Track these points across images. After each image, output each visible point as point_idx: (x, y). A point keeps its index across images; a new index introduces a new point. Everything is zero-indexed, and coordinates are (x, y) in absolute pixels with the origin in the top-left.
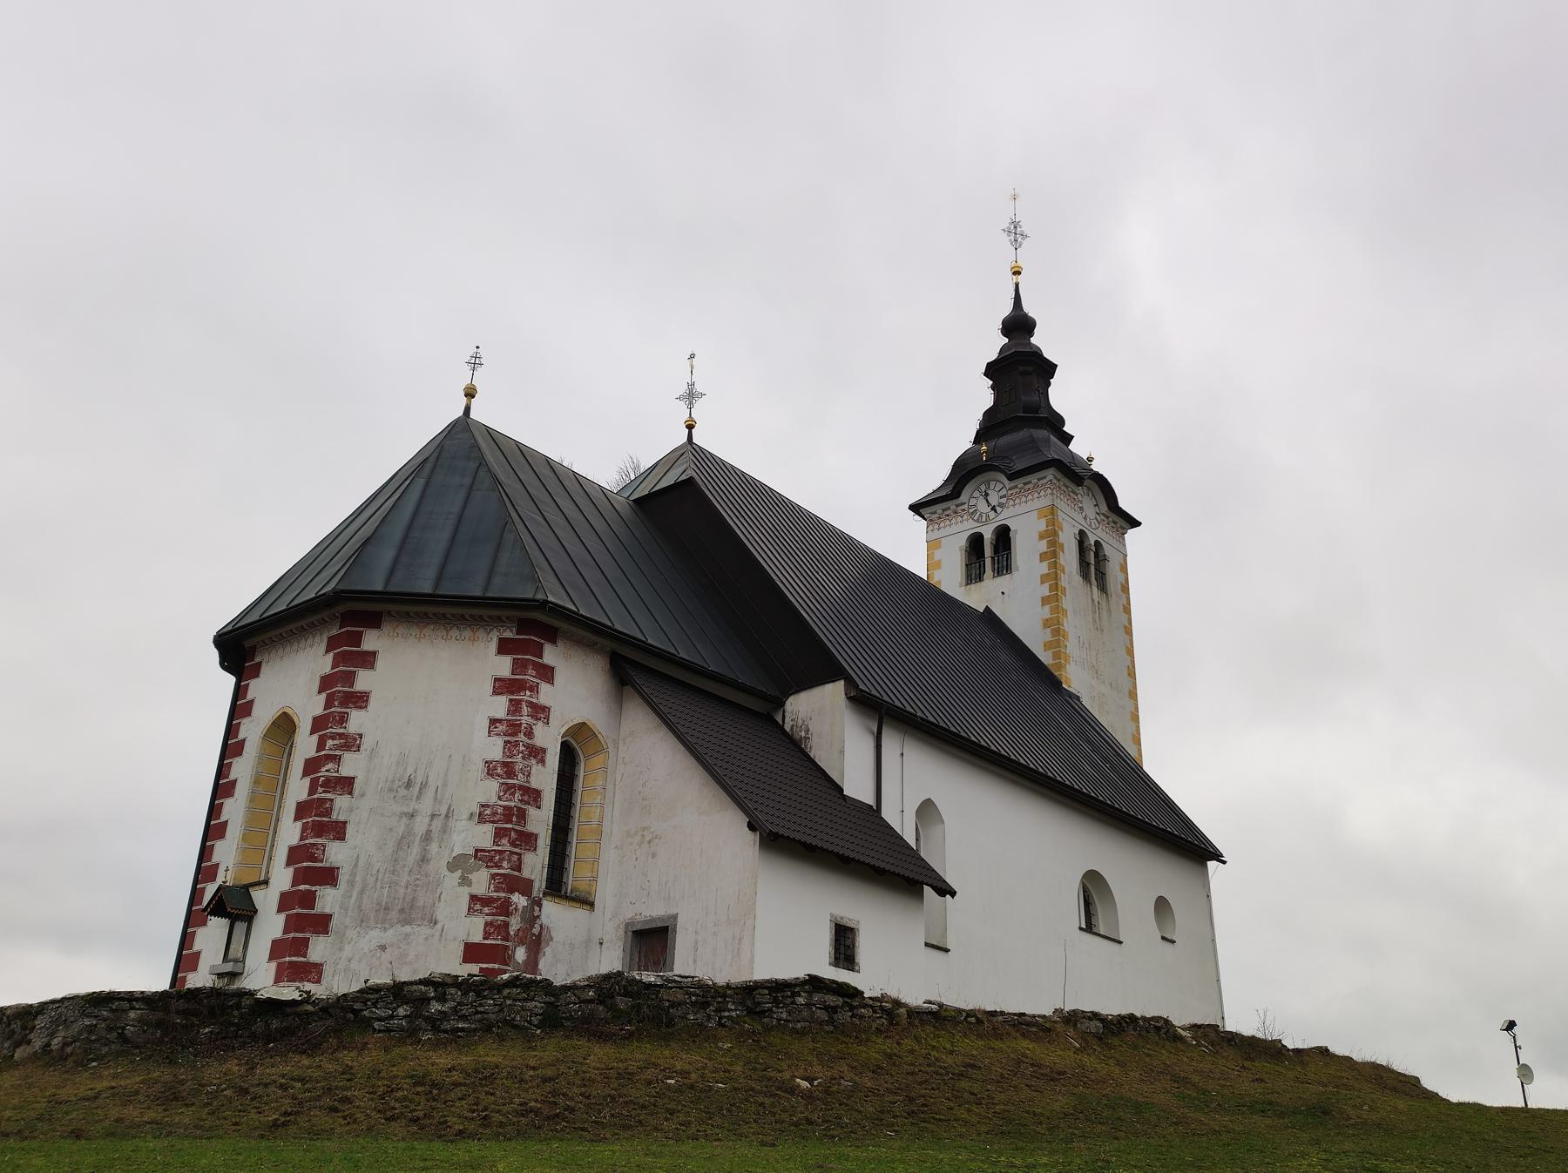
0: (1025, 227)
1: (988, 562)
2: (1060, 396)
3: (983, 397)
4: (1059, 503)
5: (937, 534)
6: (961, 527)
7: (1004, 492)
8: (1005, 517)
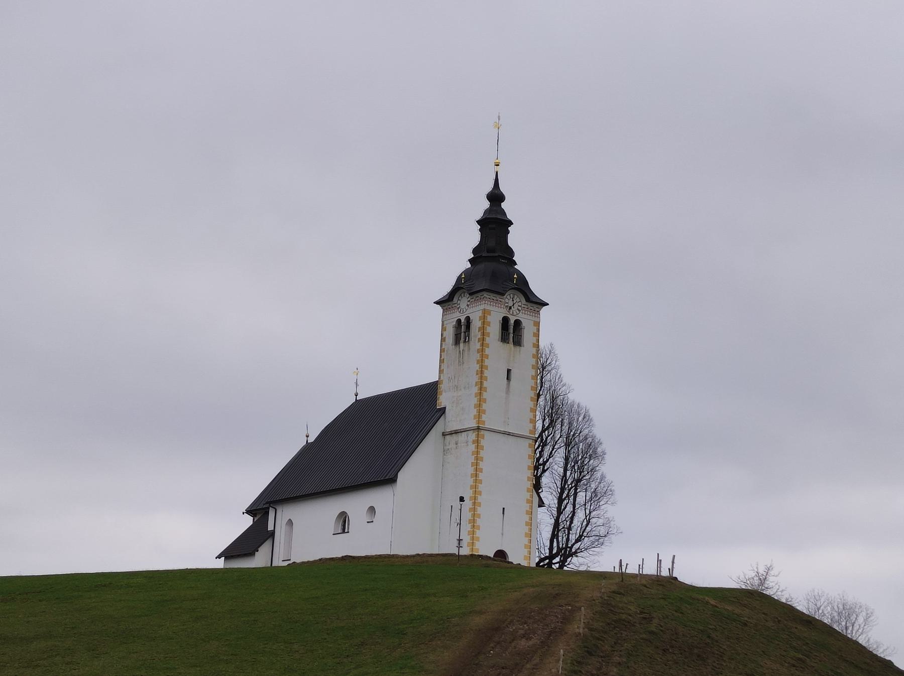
2: (513, 240)
3: (474, 237)
8: (522, 317)
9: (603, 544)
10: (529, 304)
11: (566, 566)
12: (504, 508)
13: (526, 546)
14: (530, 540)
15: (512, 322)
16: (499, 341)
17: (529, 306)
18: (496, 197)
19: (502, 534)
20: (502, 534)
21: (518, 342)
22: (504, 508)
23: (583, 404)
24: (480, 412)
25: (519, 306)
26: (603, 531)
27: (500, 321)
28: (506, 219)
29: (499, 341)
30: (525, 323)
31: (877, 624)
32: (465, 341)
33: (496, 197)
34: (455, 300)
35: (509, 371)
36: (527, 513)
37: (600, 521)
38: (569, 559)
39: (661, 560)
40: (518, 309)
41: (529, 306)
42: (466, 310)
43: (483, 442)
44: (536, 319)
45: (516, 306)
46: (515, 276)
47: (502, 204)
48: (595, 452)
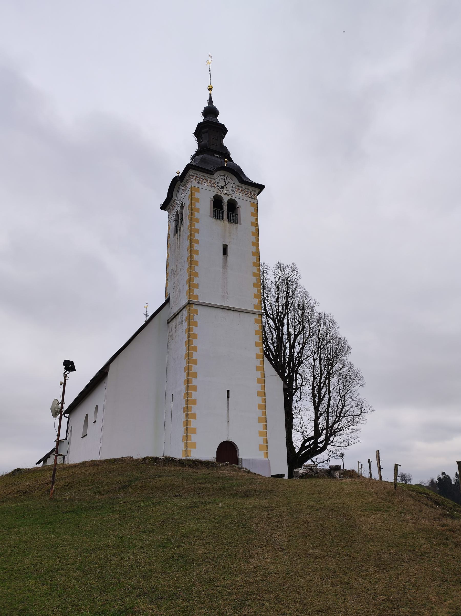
8: (236, 197)
9: (357, 422)
10: (244, 186)
11: (329, 444)
12: (228, 391)
13: (260, 434)
14: (266, 425)
16: (210, 216)
19: (228, 422)
20: (228, 422)
22: (228, 391)
23: (328, 314)
24: (192, 286)
25: (232, 187)
26: (357, 411)
29: (210, 216)
30: (240, 203)
32: (180, 228)
34: (174, 197)
36: (259, 394)
37: (354, 403)
38: (331, 438)
40: (231, 190)
43: (195, 318)
44: (253, 200)
48: (342, 348)
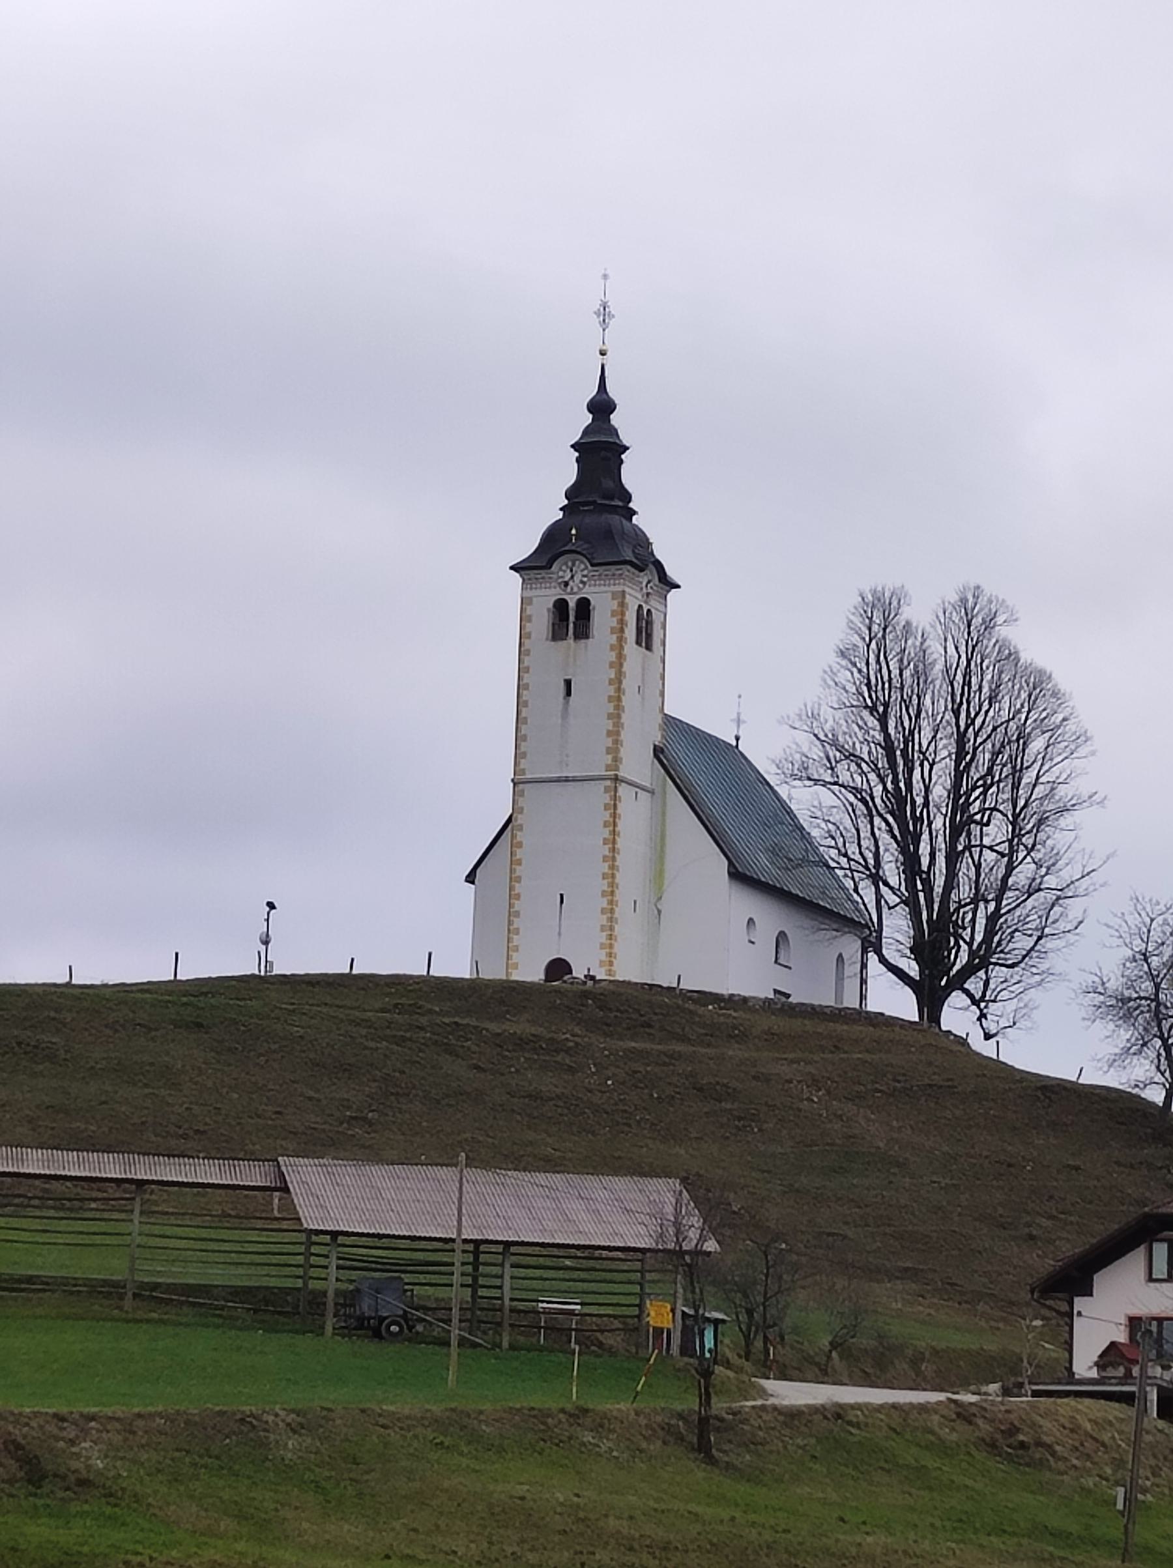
0: (612, 309)
1: (571, 626)
2: (631, 474)
3: (569, 473)
4: (627, 590)
5: (528, 594)
6: (548, 592)
7: (585, 572)
8: (588, 592)
15: (572, 605)
17: (601, 571)
18: (601, 407)
21: (583, 633)
27: (549, 610)
28: (617, 441)
31: (1093, 753)
33: (601, 407)
35: (568, 683)
39: (272, 963)
41: (544, 575)
42: (580, 589)
45: (577, 578)
46: (574, 532)
47: (612, 416)
